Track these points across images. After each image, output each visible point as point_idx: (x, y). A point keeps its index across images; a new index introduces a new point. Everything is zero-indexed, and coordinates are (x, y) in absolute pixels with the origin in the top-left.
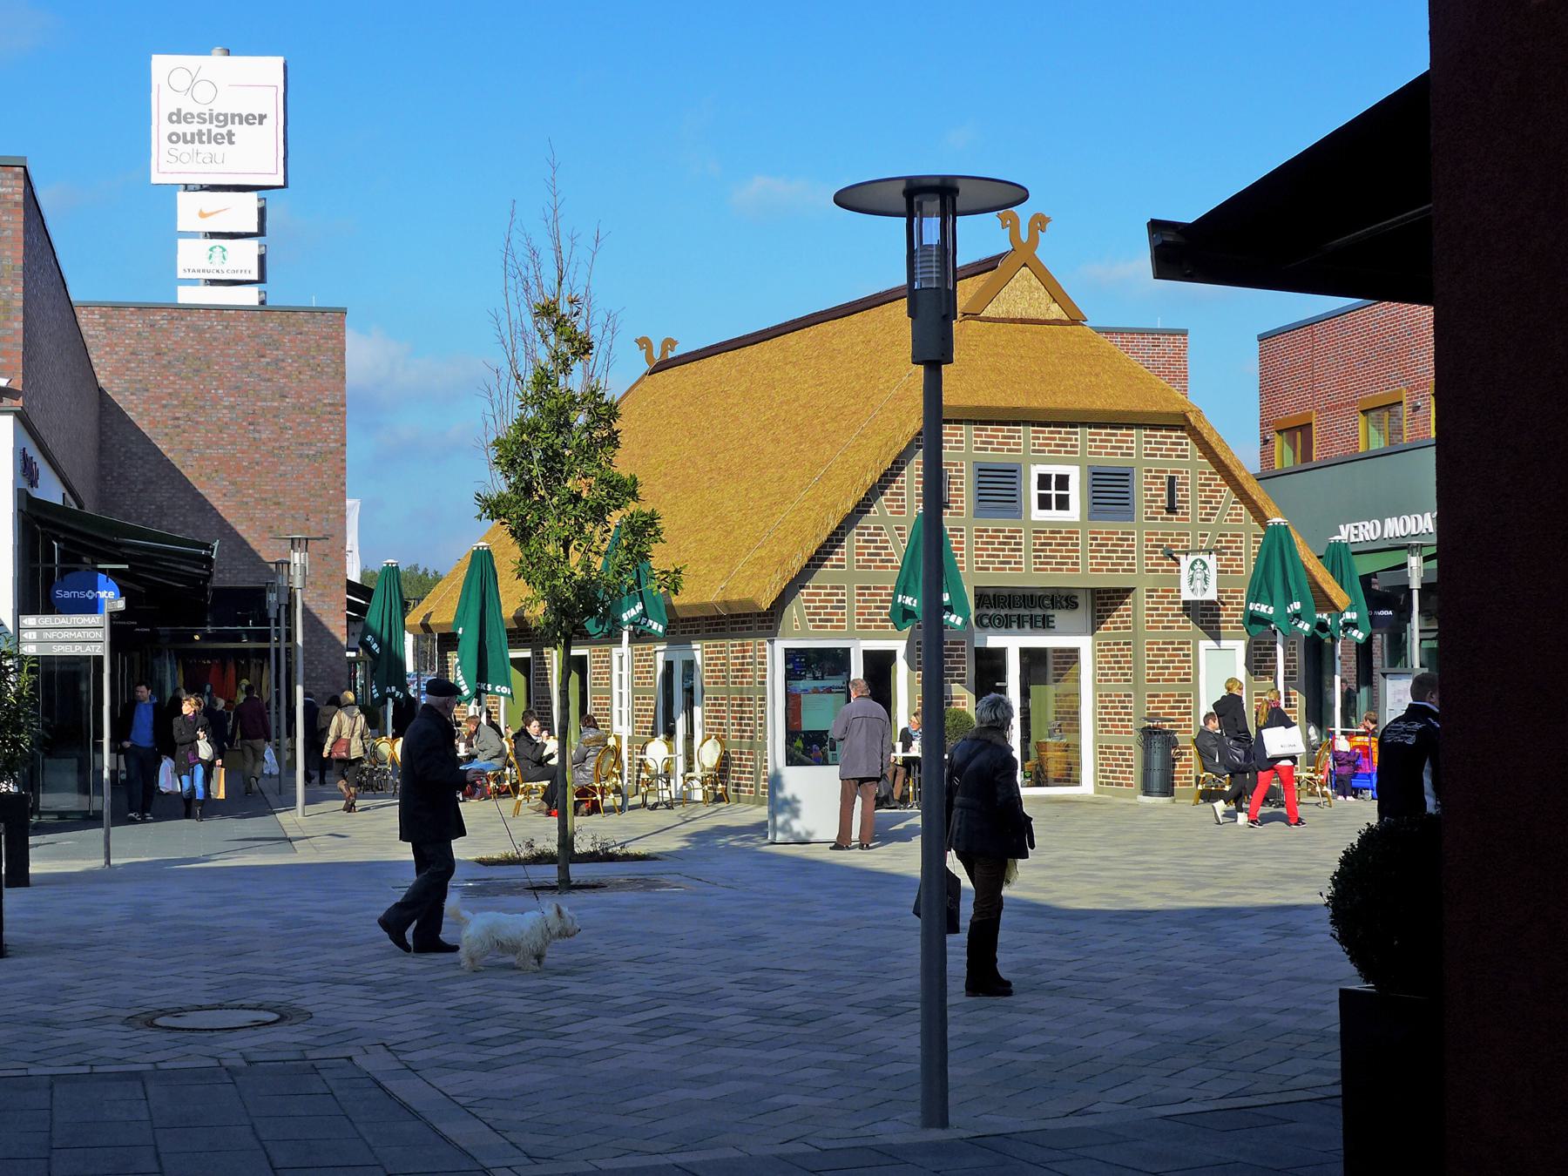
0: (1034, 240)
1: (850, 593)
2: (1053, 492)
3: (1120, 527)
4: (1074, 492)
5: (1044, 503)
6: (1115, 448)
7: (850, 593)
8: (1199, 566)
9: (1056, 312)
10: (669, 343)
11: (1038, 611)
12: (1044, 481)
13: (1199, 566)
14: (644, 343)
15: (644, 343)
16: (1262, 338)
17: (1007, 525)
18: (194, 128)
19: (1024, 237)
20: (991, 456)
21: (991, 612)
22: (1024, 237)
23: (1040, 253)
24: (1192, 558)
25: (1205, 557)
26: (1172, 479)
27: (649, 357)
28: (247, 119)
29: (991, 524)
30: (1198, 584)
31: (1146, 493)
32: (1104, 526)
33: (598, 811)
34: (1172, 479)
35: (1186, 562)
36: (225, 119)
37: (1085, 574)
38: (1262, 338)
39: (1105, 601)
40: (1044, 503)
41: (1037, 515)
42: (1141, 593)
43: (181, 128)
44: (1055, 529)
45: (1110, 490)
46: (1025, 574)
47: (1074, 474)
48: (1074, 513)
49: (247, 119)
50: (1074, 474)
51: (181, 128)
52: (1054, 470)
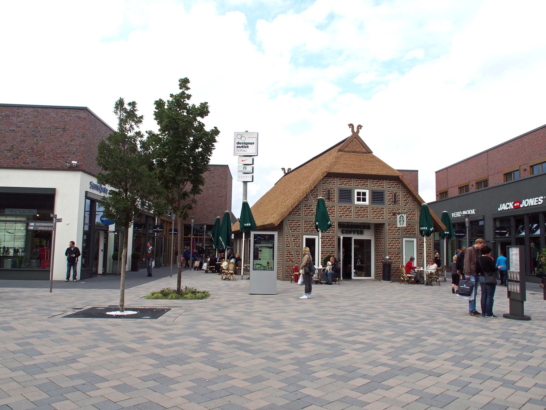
0: (358, 131)
1: (302, 223)
2: (362, 197)
3: (380, 206)
4: (367, 197)
5: (359, 200)
6: (378, 186)
7: (302, 223)
8: (402, 217)
9: (364, 150)
10: (289, 169)
11: (359, 229)
12: (359, 194)
13: (402, 217)
14: (283, 169)
15: (283, 169)
16: (436, 172)
17: (348, 205)
18: (241, 145)
19: (355, 130)
20: (343, 187)
21: (346, 229)
22: (355, 130)
23: (360, 135)
24: (400, 215)
25: (403, 215)
26: (395, 194)
27: (285, 172)
28: (251, 144)
29: (343, 205)
30: (402, 222)
31: (387, 197)
32: (376, 206)
33: (364, 270)
34: (395, 194)
35: (398, 216)
36: (247, 144)
37: (371, 219)
38: (436, 172)
39: (378, 228)
40: (359, 200)
41: (356, 202)
42: (386, 225)
43: (239, 145)
44: (362, 207)
45: (377, 197)
46: (353, 219)
47: (367, 192)
48: (367, 202)
49: (251, 144)
50: (367, 192)
51: (239, 145)
52: (362, 191)
